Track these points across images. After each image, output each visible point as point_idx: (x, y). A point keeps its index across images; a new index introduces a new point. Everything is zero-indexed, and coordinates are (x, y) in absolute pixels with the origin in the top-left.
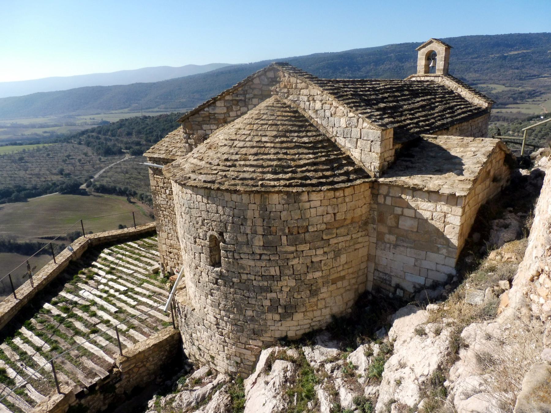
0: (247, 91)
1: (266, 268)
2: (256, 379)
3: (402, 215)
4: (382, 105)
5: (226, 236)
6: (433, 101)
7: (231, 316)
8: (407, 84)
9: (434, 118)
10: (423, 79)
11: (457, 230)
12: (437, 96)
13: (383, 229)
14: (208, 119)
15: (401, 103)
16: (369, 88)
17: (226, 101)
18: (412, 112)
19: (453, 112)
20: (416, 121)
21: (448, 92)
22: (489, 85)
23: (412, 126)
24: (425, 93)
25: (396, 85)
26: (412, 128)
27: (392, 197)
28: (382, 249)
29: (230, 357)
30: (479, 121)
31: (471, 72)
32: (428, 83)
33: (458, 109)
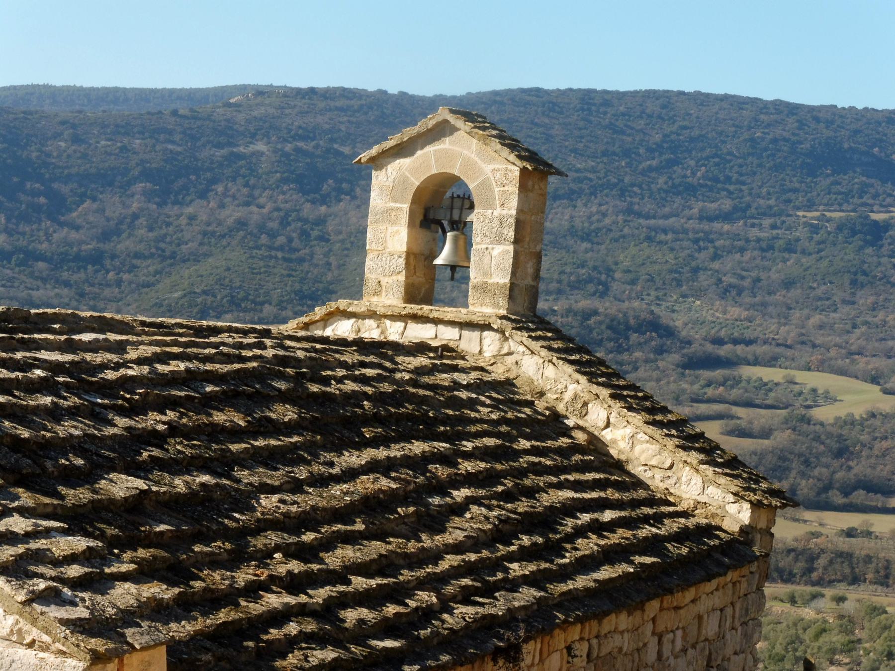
4: (121, 486)
6: (441, 471)
8: (297, 362)
9: (434, 583)
10: (394, 332)
12: (468, 446)
15: (245, 476)
16: (56, 368)
18: (309, 537)
19: (554, 549)
20: (321, 594)
21: (530, 422)
22: (801, 376)
23: (292, 628)
24: (399, 418)
25: (229, 359)
26: (291, 643)
30: (702, 607)
31: (699, 293)
32: (421, 361)
33: (581, 532)
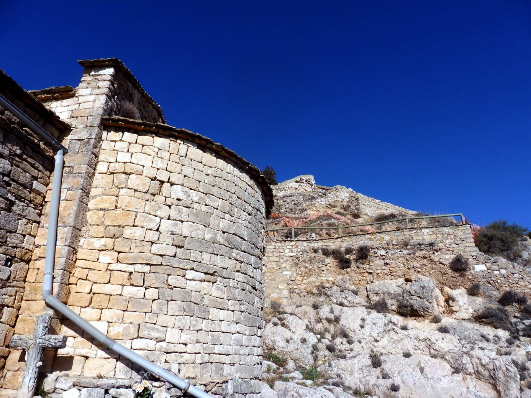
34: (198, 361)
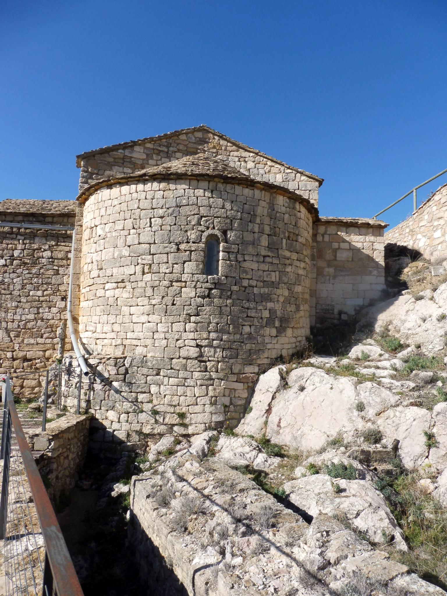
0: (171, 144)
1: (268, 272)
2: (269, 405)
3: (339, 248)
5: (231, 235)
7: (225, 337)
11: (383, 254)
13: (321, 263)
14: (122, 161)
17: (145, 148)
27: (329, 235)
28: (322, 283)
29: (216, 401)
34: (114, 344)
